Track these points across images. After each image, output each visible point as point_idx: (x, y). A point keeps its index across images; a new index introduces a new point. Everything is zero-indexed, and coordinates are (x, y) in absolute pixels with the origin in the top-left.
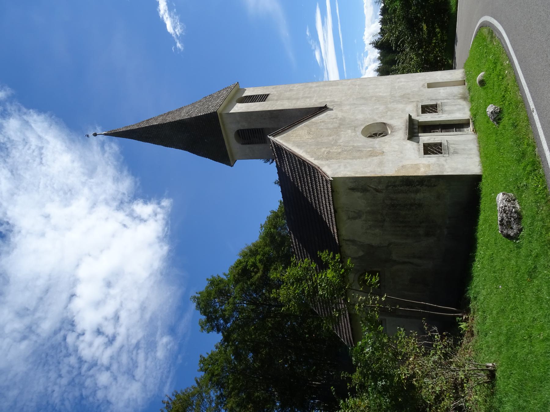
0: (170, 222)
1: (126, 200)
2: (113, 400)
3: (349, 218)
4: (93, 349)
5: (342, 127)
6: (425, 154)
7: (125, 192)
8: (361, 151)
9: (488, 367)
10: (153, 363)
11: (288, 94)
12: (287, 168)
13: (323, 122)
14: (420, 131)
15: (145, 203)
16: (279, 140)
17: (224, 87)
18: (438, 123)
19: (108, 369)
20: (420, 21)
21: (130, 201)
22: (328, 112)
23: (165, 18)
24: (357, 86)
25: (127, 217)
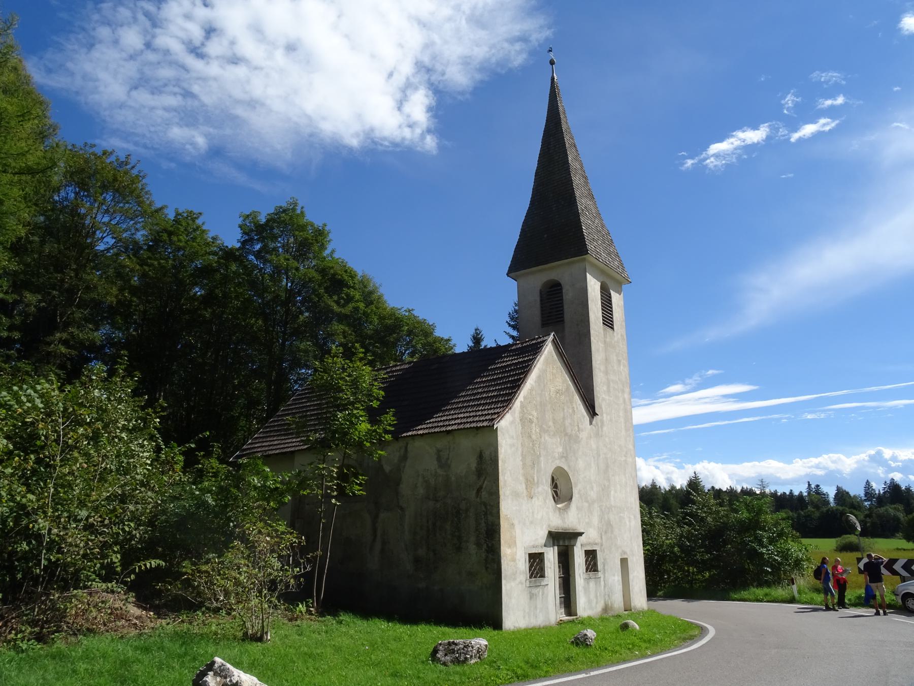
0: (398, 149)
1: (434, 78)
2: (95, 54)
3: (439, 451)
4: (180, 21)
5: (567, 438)
6: (530, 555)
7: (446, 77)
8: (533, 468)
9: (267, 633)
10: (159, 120)
11: (614, 358)
12: (508, 361)
13: (574, 411)
14: (562, 548)
15: (429, 109)
16: (549, 349)
17: (623, 262)
18: (571, 573)
19: (148, 45)
20: (709, 546)
21: (432, 84)
22: (587, 418)
23: (732, 140)
24: (624, 458)
25: (404, 80)
